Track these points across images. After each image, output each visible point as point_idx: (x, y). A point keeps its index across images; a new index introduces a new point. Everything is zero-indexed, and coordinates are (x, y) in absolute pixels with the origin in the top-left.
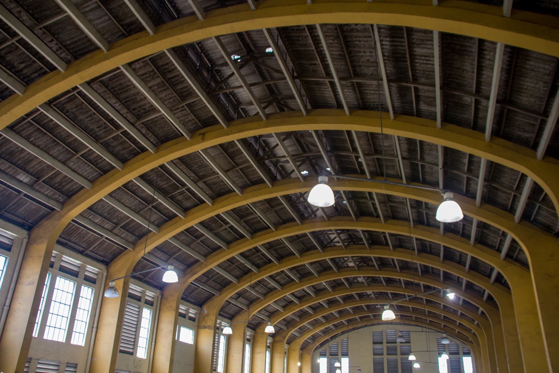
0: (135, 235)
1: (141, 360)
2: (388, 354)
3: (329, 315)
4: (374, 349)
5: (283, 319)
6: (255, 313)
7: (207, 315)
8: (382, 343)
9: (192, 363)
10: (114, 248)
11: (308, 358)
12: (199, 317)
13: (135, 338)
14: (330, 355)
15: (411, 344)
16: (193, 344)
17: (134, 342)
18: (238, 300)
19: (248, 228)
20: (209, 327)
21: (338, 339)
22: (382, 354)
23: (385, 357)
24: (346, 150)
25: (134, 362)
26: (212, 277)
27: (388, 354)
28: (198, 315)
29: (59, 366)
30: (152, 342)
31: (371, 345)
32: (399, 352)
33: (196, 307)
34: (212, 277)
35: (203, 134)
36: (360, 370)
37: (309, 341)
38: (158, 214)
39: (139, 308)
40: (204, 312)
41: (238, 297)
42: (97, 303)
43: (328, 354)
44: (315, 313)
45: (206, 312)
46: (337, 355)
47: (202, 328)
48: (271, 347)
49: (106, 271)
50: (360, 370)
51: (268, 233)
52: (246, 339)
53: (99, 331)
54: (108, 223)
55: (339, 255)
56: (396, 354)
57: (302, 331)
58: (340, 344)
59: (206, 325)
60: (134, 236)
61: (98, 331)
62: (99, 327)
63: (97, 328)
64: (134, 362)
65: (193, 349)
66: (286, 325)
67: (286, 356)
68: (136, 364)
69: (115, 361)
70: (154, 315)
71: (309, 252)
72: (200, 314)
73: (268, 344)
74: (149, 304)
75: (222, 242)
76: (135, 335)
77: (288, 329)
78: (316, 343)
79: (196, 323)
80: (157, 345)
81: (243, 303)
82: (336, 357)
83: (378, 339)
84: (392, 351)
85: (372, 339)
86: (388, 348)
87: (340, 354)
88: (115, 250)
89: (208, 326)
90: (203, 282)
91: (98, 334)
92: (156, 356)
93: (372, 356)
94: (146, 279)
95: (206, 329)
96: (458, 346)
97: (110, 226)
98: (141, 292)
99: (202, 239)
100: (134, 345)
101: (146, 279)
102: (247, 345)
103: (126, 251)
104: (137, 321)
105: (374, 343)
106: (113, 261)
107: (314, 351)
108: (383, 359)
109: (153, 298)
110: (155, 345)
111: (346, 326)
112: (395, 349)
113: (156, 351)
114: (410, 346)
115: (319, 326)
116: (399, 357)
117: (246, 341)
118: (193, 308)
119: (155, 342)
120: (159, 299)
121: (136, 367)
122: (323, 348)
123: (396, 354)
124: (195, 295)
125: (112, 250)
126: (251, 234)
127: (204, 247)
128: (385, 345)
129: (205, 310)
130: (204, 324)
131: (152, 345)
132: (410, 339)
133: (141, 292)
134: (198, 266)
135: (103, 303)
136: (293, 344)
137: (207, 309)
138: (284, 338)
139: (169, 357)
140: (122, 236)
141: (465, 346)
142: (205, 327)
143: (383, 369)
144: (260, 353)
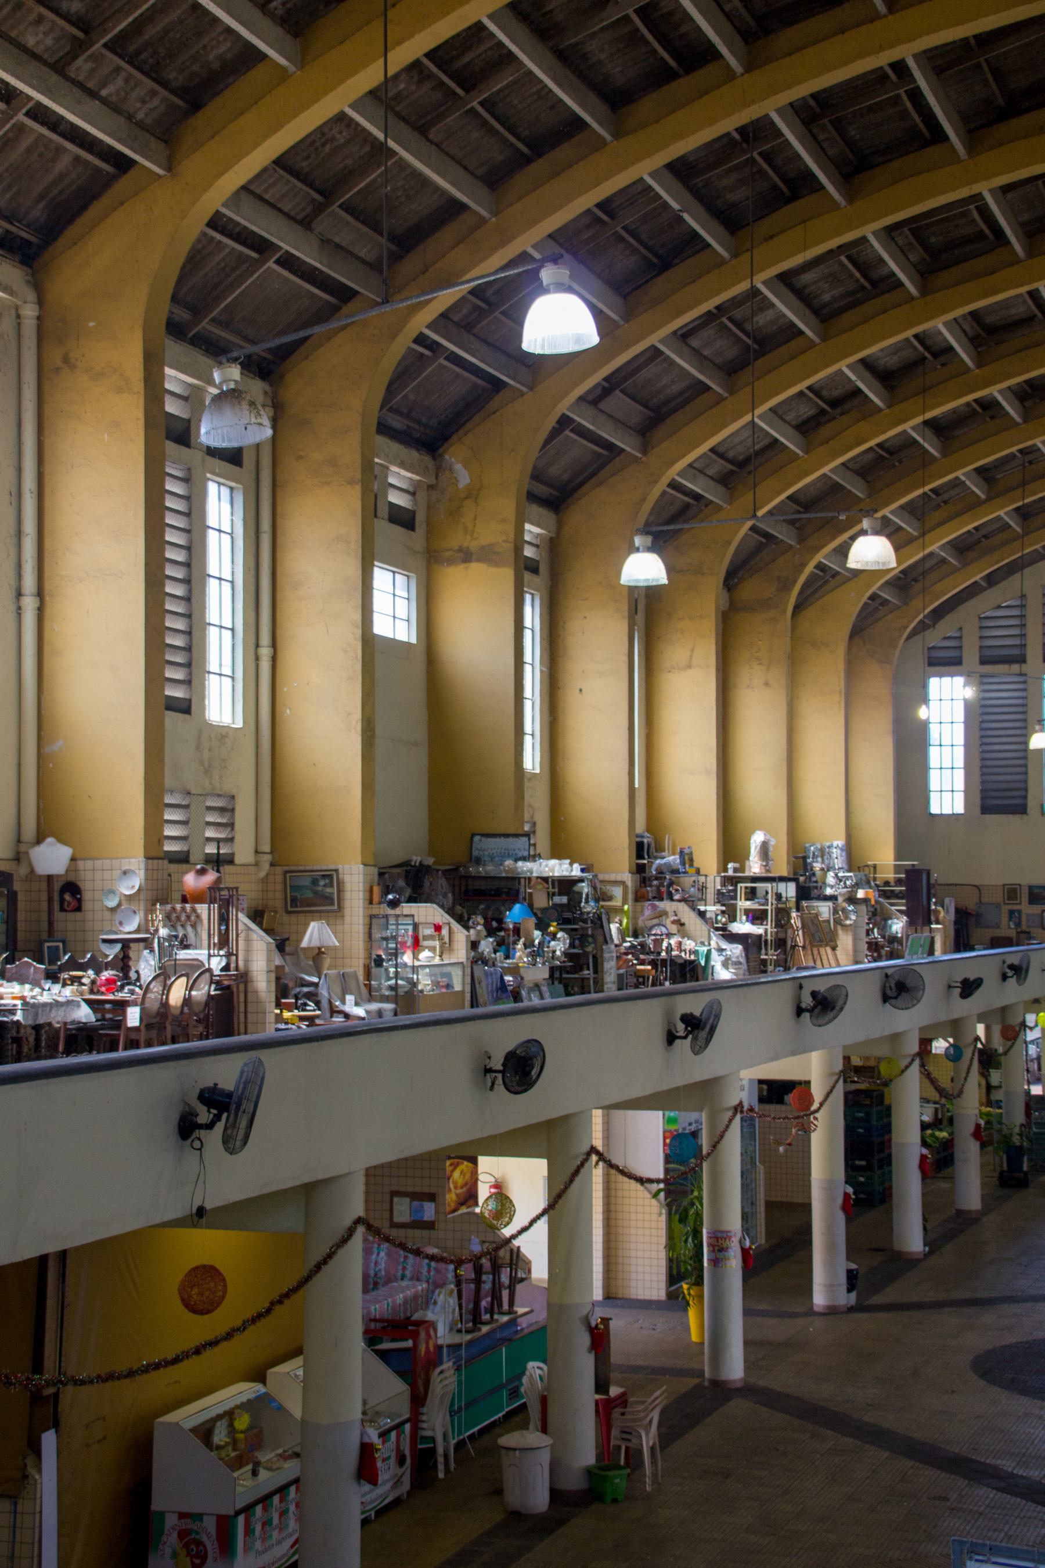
0: (164, 84)
1: (223, 734)
5: (789, 498)
6: (673, 472)
7: (473, 494)
9: (421, 733)
10: (63, 163)
13: (189, 633)
14: (983, 662)
16: (414, 640)
17: (188, 649)
18: (601, 406)
20: (487, 555)
25: (198, 747)
28: (422, 494)
29: (187, 807)
30: (257, 646)
33: (414, 455)
42: (19, 470)
43: (971, 654)
44: (945, 452)
45: (464, 478)
46: (1022, 660)
47: (451, 562)
48: (544, 569)
49: (32, 296)
52: (383, 511)
53: (57, 608)
54: (40, 19)
59: (473, 545)
60: (163, 92)
61: (48, 612)
62: (47, 586)
63: (40, 594)
65: (420, 657)
67: (541, 580)
68: (206, 754)
69: (162, 751)
70: (252, 513)
73: (529, 552)
75: (592, 98)
76: (189, 616)
78: (917, 603)
79: (417, 539)
80: (284, 656)
81: (620, 422)
82: (1015, 668)
87: (143, 1029)
88: (62, 177)
89: (483, 548)
90: (457, 324)
91: (47, 624)
92: (286, 712)
94: (205, 325)
95: (475, 566)
97: (49, 41)
98: (185, 399)
99: (498, 84)
100: (188, 665)
101: (205, 325)
102: (212, 488)
104: (188, 548)
106: (62, 241)
107: (908, 638)
110: (274, 659)
113: (283, 690)
115: (950, 519)
118: (402, 465)
119: (274, 645)
121: (207, 772)
122: (947, 627)
124: (411, 397)
125: (52, 177)
126: (746, 41)
127: (491, 130)
129: (458, 467)
130: (456, 539)
131: (257, 658)
133: (185, 399)
134: (461, 241)
135: (47, 469)
137: (466, 466)
138: (785, 586)
139: (358, 714)
140: (104, 93)
142: (466, 556)
144: (689, 666)
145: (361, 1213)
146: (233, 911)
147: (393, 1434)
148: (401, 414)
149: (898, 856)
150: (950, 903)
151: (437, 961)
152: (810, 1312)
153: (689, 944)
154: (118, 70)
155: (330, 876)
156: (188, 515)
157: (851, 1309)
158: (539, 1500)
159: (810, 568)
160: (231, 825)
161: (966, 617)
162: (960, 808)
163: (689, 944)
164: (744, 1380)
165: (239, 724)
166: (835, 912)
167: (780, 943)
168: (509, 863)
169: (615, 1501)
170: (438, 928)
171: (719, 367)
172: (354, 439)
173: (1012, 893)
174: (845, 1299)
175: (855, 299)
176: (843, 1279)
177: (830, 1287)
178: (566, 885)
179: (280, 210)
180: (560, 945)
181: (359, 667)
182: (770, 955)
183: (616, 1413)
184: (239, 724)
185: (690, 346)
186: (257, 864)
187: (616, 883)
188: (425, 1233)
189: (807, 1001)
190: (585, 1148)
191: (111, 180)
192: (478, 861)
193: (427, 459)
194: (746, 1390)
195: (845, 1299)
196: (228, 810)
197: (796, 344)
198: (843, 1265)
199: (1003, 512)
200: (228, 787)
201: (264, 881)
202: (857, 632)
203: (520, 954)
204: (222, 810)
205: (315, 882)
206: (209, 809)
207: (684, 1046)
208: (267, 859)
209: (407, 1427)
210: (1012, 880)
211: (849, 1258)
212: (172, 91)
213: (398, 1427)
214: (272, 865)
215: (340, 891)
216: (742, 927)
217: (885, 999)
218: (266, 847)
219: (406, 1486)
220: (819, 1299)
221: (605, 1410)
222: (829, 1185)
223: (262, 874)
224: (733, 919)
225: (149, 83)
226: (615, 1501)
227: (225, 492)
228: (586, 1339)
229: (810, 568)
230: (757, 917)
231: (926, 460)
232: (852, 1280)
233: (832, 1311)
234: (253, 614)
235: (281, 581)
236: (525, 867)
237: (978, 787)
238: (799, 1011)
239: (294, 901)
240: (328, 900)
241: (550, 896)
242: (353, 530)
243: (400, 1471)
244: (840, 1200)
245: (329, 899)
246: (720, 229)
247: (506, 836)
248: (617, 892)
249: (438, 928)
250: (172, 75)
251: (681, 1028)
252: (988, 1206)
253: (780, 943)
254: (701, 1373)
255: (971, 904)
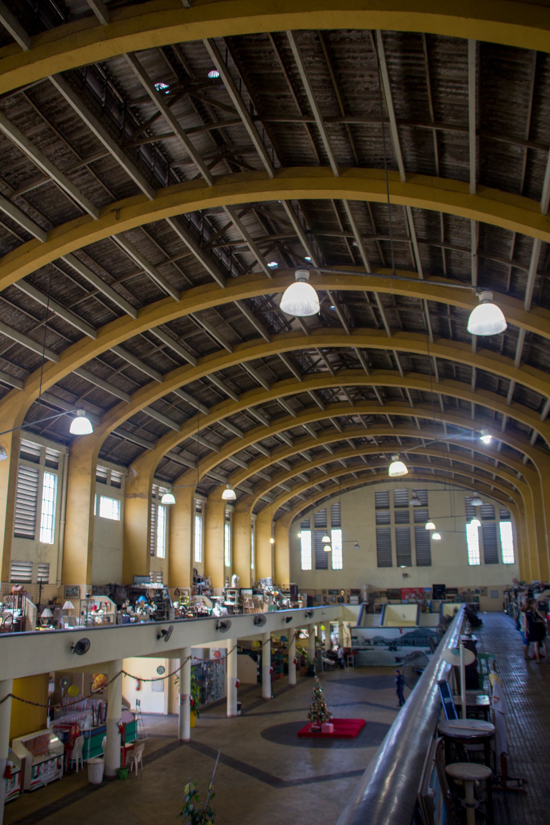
0: (23, 367)
1: (46, 546)
2: (396, 522)
3: (312, 471)
4: (377, 517)
7: (138, 478)
8: (388, 507)
9: (121, 546)
11: (284, 532)
12: (126, 482)
13: (35, 516)
14: (316, 527)
15: (429, 508)
17: (35, 521)
19: (191, 349)
20: (141, 496)
21: (326, 505)
22: (388, 523)
23: (393, 527)
24: (335, 229)
25: (37, 549)
26: (142, 423)
27: (396, 522)
28: (124, 479)
31: (373, 510)
32: (412, 519)
34: (142, 423)
35: (118, 210)
36: (357, 545)
37: (285, 508)
38: (57, 335)
39: (37, 473)
40: (133, 474)
41: (181, 451)
43: (312, 525)
44: (292, 469)
45: (135, 474)
46: (325, 526)
47: (131, 497)
48: (231, 519)
50: (357, 545)
51: (221, 356)
55: (325, 385)
56: (408, 522)
57: (275, 495)
58: (329, 511)
59: (137, 493)
60: (22, 369)
64: (37, 549)
66: (251, 488)
71: (282, 382)
72: (127, 476)
74: (53, 466)
77: (254, 492)
82: (324, 529)
83: (382, 502)
84: (402, 518)
85: (374, 502)
86: (397, 515)
87: (329, 525)
92: (68, 540)
93: (374, 526)
94: (45, 430)
95: (138, 499)
96: (493, 508)
98: (39, 451)
100: (34, 526)
101: (45, 430)
103: (13, 391)
104: (37, 492)
105: (377, 508)
107: (293, 522)
108: (390, 529)
109: (57, 457)
110: (65, 524)
111: (338, 485)
112: (407, 515)
113: (67, 533)
114: (427, 511)
116: (412, 526)
117: (195, 513)
118: (116, 470)
119: (65, 520)
120: (67, 458)
121: (40, 557)
122: (306, 517)
123: (408, 522)
128: (392, 510)
129: (134, 471)
130: (133, 491)
131: (60, 524)
132: (427, 501)
133: (39, 451)
136: (262, 513)
138: (250, 505)
139: (87, 540)
140: (4, 369)
141: (503, 507)
142: (135, 496)
143: (390, 543)
144: (216, 528)
145: (10, 691)
146: (24, 597)
147: (56, 760)
148: (115, 456)
149: (291, 581)
150: (306, 595)
151: (105, 613)
152: (226, 717)
153: (206, 608)
154: (7, 363)
155: (77, 588)
156: (37, 483)
157: (238, 716)
158: (99, 779)
159: (257, 500)
160: (48, 572)
161: (309, 515)
162: (310, 568)
163: (206, 608)
164: (190, 739)
165: (53, 543)
166: (263, 598)
167: (240, 607)
168: (143, 584)
169: (124, 779)
170: (106, 603)
171: (216, 445)
172: (90, 462)
173: (324, 591)
174: (236, 712)
175: (252, 427)
176: (236, 707)
177: (232, 709)
178: (160, 591)
179: (65, 401)
180: (153, 609)
181: (88, 526)
182: (236, 611)
183: (128, 752)
184: (53, 543)
185: (206, 439)
186: (57, 584)
187: (186, 590)
188: (100, 695)
189: (220, 625)
190: (119, 671)
191: (9, 391)
192: (136, 584)
193: (125, 469)
194: (190, 743)
195: (236, 712)
196: (47, 568)
197: (236, 439)
198: (236, 703)
199: (315, 485)
200: (47, 561)
201: (59, 589)
202: (275, 520)
203: (265, 609)
204: (45, 568)
205: (73, 589)
206: (40, 567)
207: (162, 639)
208: (60, 583)
209: (62, 757)
210: (324, 588)
211: (238, 700)
212: (26, 369)
213: (58, 757)
214: (62, 584)
215: (80, 592)
216: (228, 603)
217: (255, 623)
218: (60, 579)
219: (61, 774)
220: (229, 713)
221: (124, 751)
222: (232, 679)
223: (58, 587)
224: (226, 599)
225: (18, 367)
226: (124, 779)
227: (52, 477)
228: (117, 730)
229: (257, 500)
230: (233, 600)
231: (287, 472)
232: (239, 707)
233: (232, 717)
234: (59, 511)
235: (68, 501)
236: (148, 586)
237: (314, 562)
238: (217, 628)
239: (67, 595)
240: (76, 595)
241: (155, 594)
242: (88, 487)
243: (58, 771)
244: (235, 683)
245: (76, 595)
246: (206, 409)
247: (144, 576)
248: (186, 593)
249: (106, 603)
250: (25, 364)
251: (161, 634)
252: (298, 683)
253: (240, 607)
254: (177, 737)
255: (312, 594)
